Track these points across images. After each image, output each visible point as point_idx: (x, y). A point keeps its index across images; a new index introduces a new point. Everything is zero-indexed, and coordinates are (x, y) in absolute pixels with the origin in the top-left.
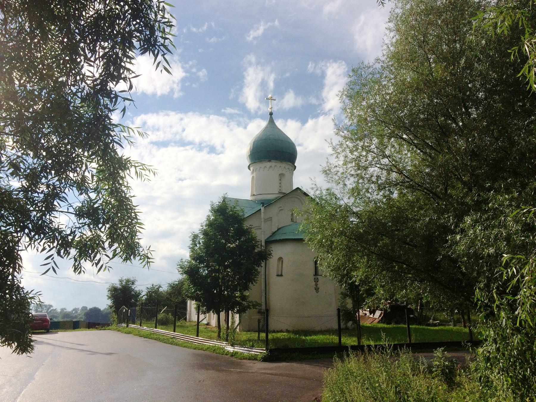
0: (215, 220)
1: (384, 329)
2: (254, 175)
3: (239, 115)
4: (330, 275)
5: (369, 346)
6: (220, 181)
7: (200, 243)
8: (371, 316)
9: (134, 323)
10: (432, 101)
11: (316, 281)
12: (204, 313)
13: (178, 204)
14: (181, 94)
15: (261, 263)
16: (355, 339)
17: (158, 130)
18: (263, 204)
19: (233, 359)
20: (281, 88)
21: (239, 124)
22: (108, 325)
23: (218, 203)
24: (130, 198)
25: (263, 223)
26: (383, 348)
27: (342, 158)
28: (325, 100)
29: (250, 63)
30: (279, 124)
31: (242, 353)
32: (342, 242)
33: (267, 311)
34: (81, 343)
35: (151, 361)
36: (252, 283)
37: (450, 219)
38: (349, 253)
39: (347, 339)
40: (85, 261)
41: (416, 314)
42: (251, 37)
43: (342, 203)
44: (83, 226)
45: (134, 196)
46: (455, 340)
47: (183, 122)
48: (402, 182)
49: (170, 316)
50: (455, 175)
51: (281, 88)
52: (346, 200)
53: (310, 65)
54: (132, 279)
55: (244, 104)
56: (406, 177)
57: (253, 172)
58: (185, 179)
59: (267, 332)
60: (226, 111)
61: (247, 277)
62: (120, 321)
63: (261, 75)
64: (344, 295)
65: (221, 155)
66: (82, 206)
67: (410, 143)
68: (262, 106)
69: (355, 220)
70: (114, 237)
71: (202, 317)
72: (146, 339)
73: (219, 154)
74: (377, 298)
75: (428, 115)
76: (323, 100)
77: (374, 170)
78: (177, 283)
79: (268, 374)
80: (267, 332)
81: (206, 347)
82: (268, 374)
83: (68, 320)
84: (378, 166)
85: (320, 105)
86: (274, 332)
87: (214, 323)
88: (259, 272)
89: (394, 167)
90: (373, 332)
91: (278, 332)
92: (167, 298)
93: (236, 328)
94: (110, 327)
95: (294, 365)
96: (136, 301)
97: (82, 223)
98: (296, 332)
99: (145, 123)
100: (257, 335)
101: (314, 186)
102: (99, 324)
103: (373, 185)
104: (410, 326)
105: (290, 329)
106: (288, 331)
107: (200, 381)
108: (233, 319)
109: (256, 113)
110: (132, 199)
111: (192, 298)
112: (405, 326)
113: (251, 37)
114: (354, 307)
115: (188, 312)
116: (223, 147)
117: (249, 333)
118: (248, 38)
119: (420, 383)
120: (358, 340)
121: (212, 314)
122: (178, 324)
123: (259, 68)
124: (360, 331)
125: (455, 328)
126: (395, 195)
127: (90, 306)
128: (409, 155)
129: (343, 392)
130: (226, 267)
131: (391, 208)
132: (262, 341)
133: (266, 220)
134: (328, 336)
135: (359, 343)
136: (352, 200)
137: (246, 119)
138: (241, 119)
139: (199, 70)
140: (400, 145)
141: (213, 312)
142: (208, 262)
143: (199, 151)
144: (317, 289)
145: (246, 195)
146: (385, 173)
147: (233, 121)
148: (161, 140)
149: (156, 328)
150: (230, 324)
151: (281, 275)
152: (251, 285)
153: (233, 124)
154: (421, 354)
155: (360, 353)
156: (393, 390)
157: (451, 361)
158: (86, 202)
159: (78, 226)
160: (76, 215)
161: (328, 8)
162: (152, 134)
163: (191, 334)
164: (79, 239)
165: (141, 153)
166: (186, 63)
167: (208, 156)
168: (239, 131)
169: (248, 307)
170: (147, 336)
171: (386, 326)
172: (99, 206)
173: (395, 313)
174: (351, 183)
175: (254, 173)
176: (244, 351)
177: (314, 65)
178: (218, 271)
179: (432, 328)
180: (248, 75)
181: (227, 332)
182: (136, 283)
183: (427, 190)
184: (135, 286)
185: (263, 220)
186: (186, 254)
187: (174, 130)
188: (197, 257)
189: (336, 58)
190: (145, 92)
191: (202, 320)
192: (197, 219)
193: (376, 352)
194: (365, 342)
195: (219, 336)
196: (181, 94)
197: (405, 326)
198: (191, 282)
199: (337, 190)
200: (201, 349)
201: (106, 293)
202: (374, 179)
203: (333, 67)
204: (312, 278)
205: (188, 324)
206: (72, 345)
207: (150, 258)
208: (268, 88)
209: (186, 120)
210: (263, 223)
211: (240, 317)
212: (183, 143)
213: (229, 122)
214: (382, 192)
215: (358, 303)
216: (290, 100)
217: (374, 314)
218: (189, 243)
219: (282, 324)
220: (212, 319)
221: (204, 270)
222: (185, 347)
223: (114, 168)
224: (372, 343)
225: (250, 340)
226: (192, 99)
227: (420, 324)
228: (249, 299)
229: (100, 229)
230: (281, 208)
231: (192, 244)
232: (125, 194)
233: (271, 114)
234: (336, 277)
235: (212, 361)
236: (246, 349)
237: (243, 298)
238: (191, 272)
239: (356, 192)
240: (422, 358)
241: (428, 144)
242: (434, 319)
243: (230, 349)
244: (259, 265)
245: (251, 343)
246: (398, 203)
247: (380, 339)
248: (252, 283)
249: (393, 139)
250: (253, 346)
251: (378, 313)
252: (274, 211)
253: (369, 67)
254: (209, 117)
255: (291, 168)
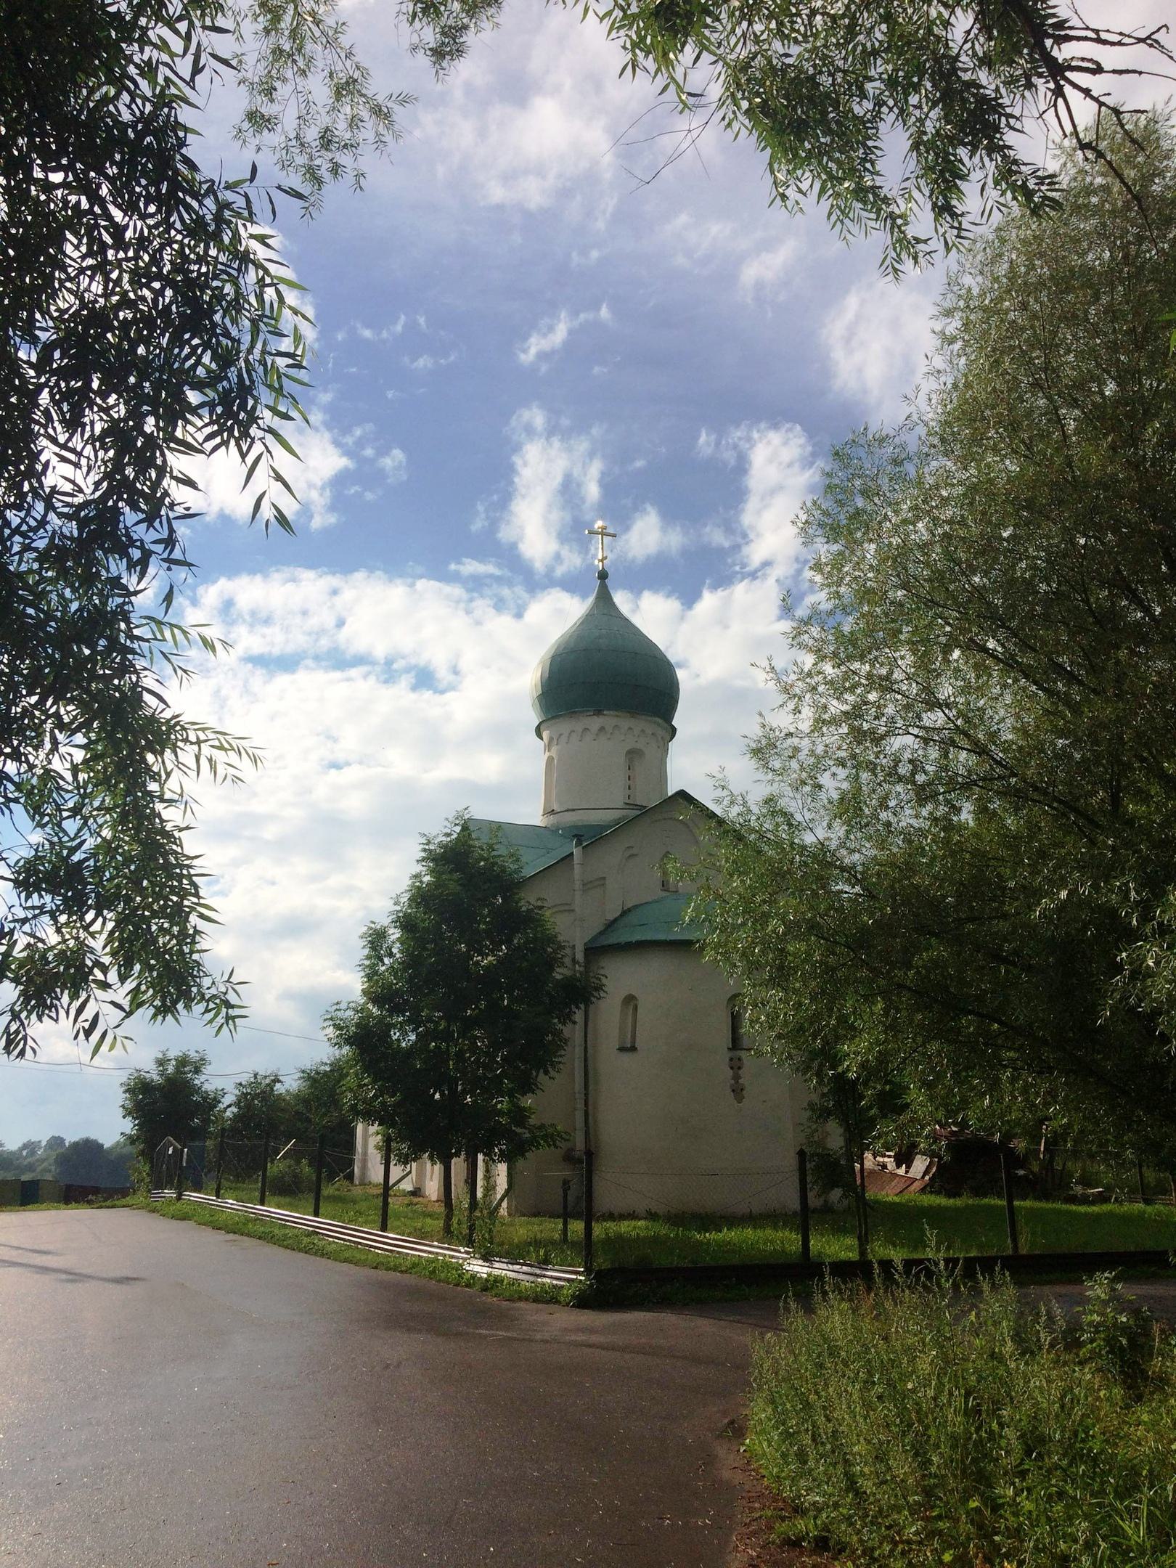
0: (437, 885)
1: (934, 1215)
2: (554, 752)
3: (499, 580)
4: (773, 1053)
5: (886, 1265)
6: (449, 769)
7: (391, 955)
8: (902, 1171)
9: (198, 1188)
10: (1073, 543)
11: (736, 1065)
12: (405, 1160)
13: (327, 836)
14: (332, 519)
15: (571, 1013)
16: (851, 1241)
17: (268, 621)
18: (579, 838)
19: (490, 1299)
20: (621, 501)
21: (500, 605)
22: (124, 1193)
23: (441, 838)
24: (176, 834)
25: (578, 894)
26: (929, 1275)
27: (808, 713)
28: (752, 536)
29: (530, 431)
30: (621, 599)
31: (513, 1282)
32: (809, 954)
33: (590, 1154)
34: (43, 1248)
35: (247, 1306)
36: (546, 1072)
37: (1126, 890)
38: (831, 985)
39: (828, 1242)
40: (40, 1018)
41: (1036, 1169)
42: (533, 351)
43: (809, 839)
44: (35, 917)
45: (188, 828)
46: (1150, 1245)
47: (338, 600)
48: (984, 779)
49: (306, 1169)
50: (1143, 760)
51: (621, 501)
52: (821, 833)
53: (703, 438)
54: (194, 1056)
55: (513, 547)
56: (999, 763)
57: (549, 746)
58: (348, 764)
59: (589, 1217)
60: (461, 568)
61: (533, 1053)
62: (159, 1183)
63: (560, 465)
64: (821, 1114)
65: (449, 696)
66: (37, 857)
67: (1009, 663)
68: (565, 552)
69: (847, 888)
70: (131, 948)
71: (396, 1172)
72: (231, 1236)
73: (442, 692)
74: (912, 1120)
75: (1059, 584)
76: (745, 536)
77: (903, 743)
78: (328, 1069)
79: (590, 1346)
80: (589, 1217)
81: (408, 1263)
82: (590, 1346)
83: (10, 1176)
84: (916, 731)
85: (737, 548)
86: (611, 1217)
87: (433, 1188)
88: (566, 1041)
89: (966, 731)
90: (903, 1220)
91: (622, 1217)
92: (297, 1113)
93: (499, 1204)
94: (129, 1200)
95: (669, 1319)
96: (206, 1121)
97: (33, 908)
98: (677, 1219)
99: (227, 606)
100: (560, 1226)
101: (719, 793)
102: (96, 1191)
103: (899, 788)
104: (1016, 1203)
105: (661, 1209)
106: (652, 1216)
107: (387, 1366)
108: (488, 1176)
109: (550, 570)
110: (183, 835)
111: (369, 1116)
112: (1000, 1203)
113: (533, 351)
114: (849, 1142)
115: (358, 1158)
116: (456, 672)
117: (536, 1220)
118: (523, 357)
119: (1040, 1384)
120: (861, 1245)
121: (429, 1164)
122: (328, 1190)
123: (556, 442)
124: (865, 1216)
125: (1149, 1209)
126: (966, 815)
127: (71, 1136)
128: (1008, 699)
129: (807, 1405)
130: (468, 1025)
131: (953, 854)
132: (574, 1245)
133: (587, 886)
134: (769, 1232)
135: (863, 1253)
136: (840, 830)
137: (520, 590)
138: (506, 592)
139: (383, 452)
140: (980, 668)
141: (431, 1158)
142: (416, 1010)
143: (386, 682)
144: (738, 1091)
145: (529, 811)
146: (934, 753)
147: (482, 596)
148: (276, 651)
149: (262, 1203)
150: (479, 1194)
151: (633, 1049)
152: (542, 1077)
153: (482, 606)
154: (1047, 1289)
155: (859, 1283)
156: (959, 1402)
157: (1136, 1313)
158: (47, 846)
159: (21, 914)
160: (17, 883)
161: (751, 273)
162: (250, 632)
163: (366, 1223)
164: (24, 954)
165: (218, 691)
166: (347, 430)
167: (413, 696)
168: (501, 624)
169: (533, 1143)
170: (237, 1228)
171: (942, 1201)
172: (86, 859)
173: (967, 1164)
174: (834, 783)
175: (554, 749)
176: (521, 1277)
177: (713, 437)
178: (446, 1036)
179: (1083, 1209)
180: (525, 464)
181: (470, 1218)
182: (208, 1070)
183: (1060, 802)
184: (203, 1078)
185: (578, 885)
186: (348, 984)
187: (313, 622)
188: (380, 993)
189: (776, 415)
190: (227, 512)
191: (399, 1181)
192: (382, 882)
193: (909, 1287)
194: (881, 1250)
195: (447, 1229)
196: (332, 519)
197: (1000, 1203)
198: (366, 1069)
199: (793, 803)
200: (395, 1269)
201: (119, 1097)
202: (904, 770)
203: (769, 443)
204: (724, 1055)
205: (357, 1191)
206: (14, 1253)
207: (233, 1007)
208: (583, 500)
209: (348, 595)
210: (578, 894)
211: (509, 1168)
212: (339, 660)
213: (471, 600)
214: (929, 807)
215: (858, 1138)
216: (647, 535)
217: (908, 1167)
218: (360, 951)
219: (634, 1196)
220: (429, 1177)
221: (405, 1034)
222: (346, 1261)
223: (131, 739)
224: (897, 1255)
225: (537, 1243)
226: (367, 533)
227: (1046, 1196)
228: (533, 1121)
229: (86, 928)
230: (631, 852)
231: (368, 957)
232: (162, 821)
233: (603, 576)
234: (790, 1057)
235: (425, 1305)
236: (525, 1268)
237: (519, 1116)
238: (365, 1039)
239: (849, 807)
240: (1052, 1303)
241: (1060, 666)
242: (1086, 1181)
243: (479, 1268)
244: (567, 1018)
245: (542, 1252)
246: (974, 841)
247: (920, 1243)
248: (546, 1072)
249: (956, 654)
250: (545, 1262)
251: (920, 1164)
252: (610, 857)
253: (882, 441)
254: (412, 585)
255: (660, 732)
